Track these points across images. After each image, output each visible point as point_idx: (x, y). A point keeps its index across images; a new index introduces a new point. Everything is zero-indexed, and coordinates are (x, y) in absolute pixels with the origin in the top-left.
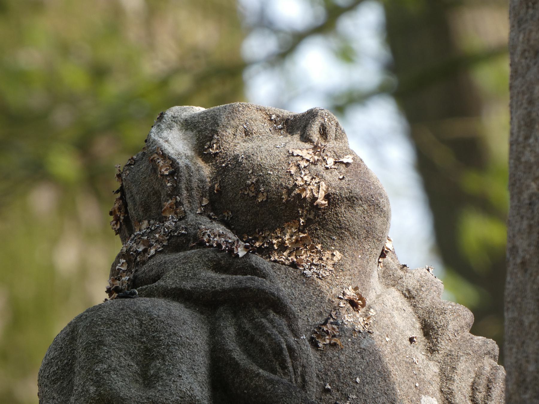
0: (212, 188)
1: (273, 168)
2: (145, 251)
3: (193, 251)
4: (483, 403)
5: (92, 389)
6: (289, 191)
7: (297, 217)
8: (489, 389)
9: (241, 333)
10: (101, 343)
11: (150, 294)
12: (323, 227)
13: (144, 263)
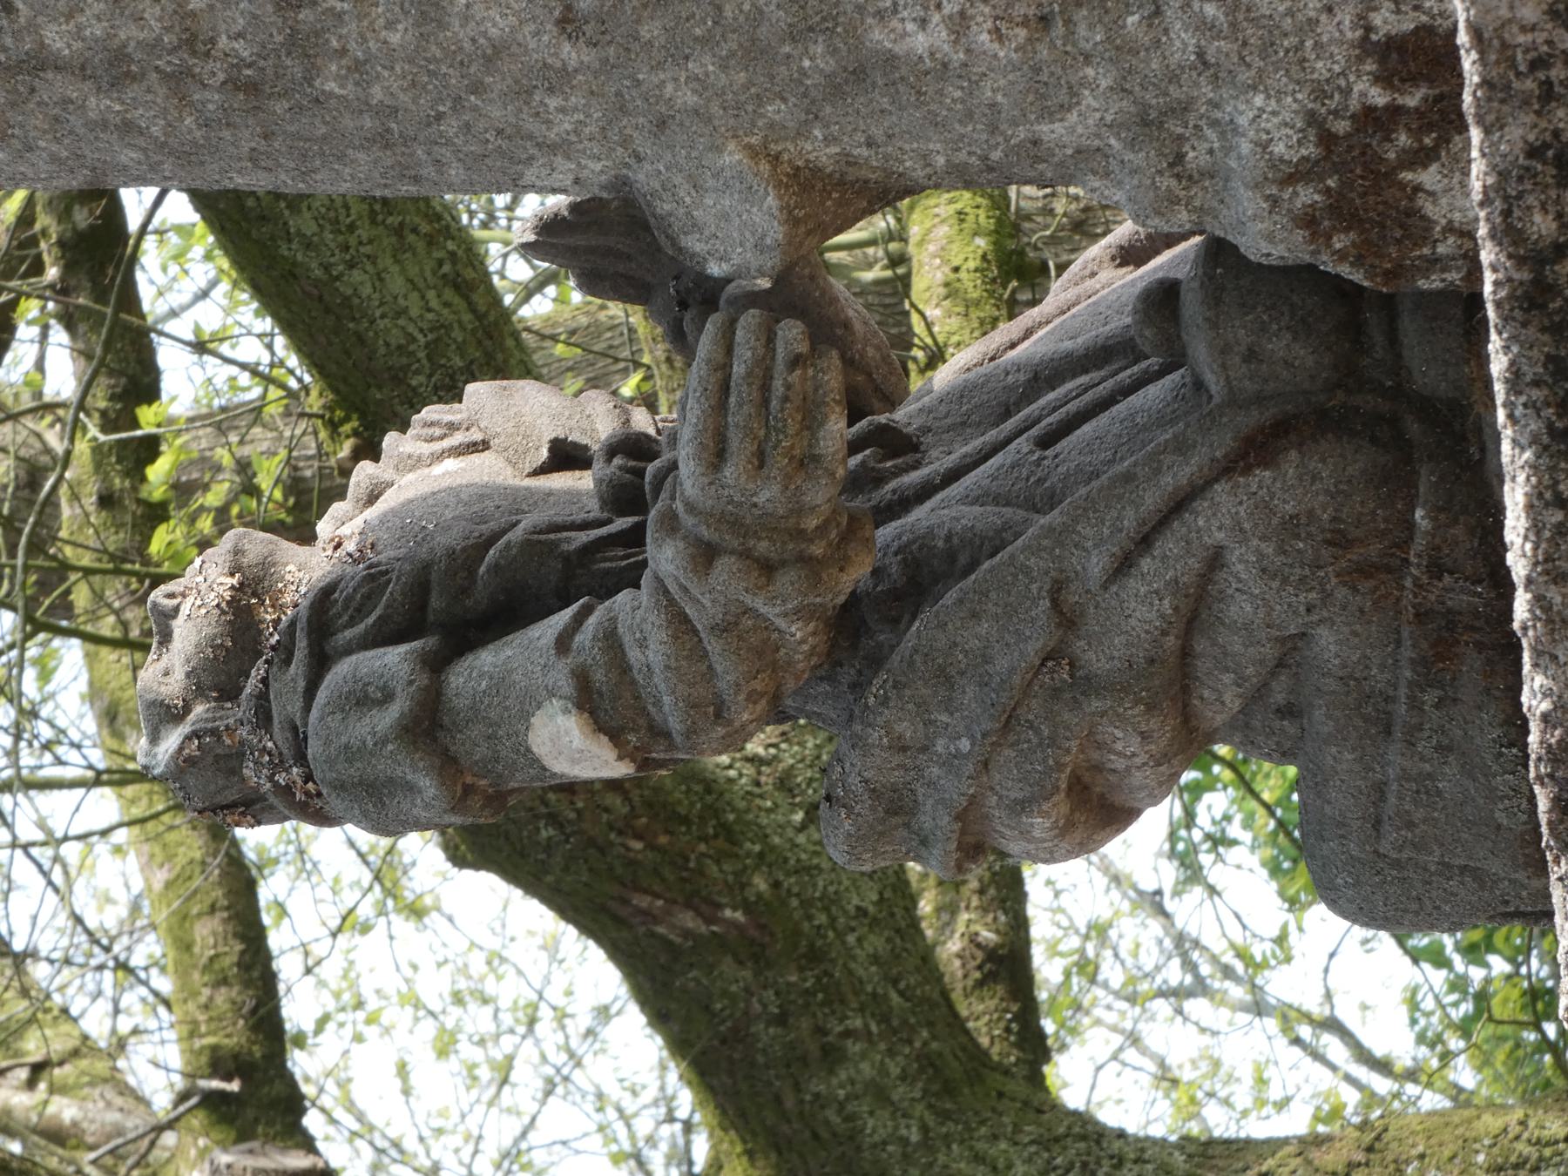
0: (216, 699)
1: (200, 632)
2: (270, 754)
3: (268, 535)
4: (464, 1171)
5: (390, 747)
6: (223, 613)
7: (249, 605)
8: (432, 424)
9: (352, 623)
10: (347, 747)
11: (306, 725)
12: (261, 580)
13: (281, 754)
